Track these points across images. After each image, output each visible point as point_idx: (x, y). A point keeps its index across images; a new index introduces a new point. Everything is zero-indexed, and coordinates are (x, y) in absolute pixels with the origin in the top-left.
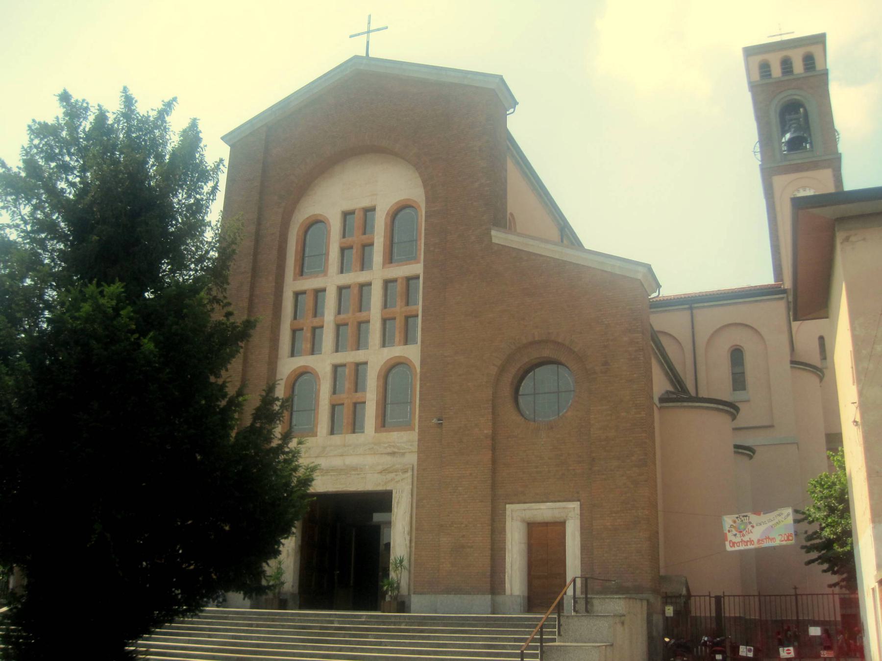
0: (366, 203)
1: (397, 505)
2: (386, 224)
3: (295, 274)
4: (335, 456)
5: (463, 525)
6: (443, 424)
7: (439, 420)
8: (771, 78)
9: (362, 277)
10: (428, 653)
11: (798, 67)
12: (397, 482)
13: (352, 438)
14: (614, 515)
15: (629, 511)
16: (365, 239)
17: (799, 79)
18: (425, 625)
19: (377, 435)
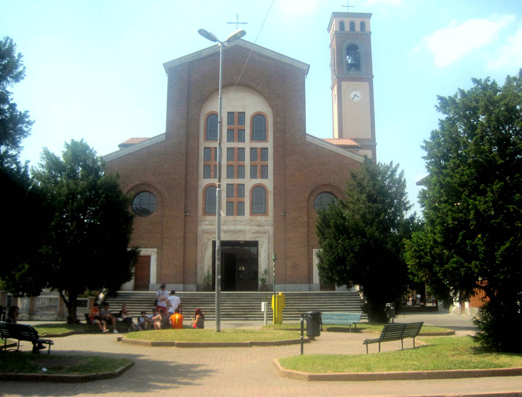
0: (241, 110)
3: (204, 139)
4: (231, 225)
7: (284, 213)
8: (344, 30)
9: (240, 145)
10: (121, 301)
12: (261, 237)
13: (239, 218)
17: (358, 34)
18: (306, 296)
19: (251, 217)
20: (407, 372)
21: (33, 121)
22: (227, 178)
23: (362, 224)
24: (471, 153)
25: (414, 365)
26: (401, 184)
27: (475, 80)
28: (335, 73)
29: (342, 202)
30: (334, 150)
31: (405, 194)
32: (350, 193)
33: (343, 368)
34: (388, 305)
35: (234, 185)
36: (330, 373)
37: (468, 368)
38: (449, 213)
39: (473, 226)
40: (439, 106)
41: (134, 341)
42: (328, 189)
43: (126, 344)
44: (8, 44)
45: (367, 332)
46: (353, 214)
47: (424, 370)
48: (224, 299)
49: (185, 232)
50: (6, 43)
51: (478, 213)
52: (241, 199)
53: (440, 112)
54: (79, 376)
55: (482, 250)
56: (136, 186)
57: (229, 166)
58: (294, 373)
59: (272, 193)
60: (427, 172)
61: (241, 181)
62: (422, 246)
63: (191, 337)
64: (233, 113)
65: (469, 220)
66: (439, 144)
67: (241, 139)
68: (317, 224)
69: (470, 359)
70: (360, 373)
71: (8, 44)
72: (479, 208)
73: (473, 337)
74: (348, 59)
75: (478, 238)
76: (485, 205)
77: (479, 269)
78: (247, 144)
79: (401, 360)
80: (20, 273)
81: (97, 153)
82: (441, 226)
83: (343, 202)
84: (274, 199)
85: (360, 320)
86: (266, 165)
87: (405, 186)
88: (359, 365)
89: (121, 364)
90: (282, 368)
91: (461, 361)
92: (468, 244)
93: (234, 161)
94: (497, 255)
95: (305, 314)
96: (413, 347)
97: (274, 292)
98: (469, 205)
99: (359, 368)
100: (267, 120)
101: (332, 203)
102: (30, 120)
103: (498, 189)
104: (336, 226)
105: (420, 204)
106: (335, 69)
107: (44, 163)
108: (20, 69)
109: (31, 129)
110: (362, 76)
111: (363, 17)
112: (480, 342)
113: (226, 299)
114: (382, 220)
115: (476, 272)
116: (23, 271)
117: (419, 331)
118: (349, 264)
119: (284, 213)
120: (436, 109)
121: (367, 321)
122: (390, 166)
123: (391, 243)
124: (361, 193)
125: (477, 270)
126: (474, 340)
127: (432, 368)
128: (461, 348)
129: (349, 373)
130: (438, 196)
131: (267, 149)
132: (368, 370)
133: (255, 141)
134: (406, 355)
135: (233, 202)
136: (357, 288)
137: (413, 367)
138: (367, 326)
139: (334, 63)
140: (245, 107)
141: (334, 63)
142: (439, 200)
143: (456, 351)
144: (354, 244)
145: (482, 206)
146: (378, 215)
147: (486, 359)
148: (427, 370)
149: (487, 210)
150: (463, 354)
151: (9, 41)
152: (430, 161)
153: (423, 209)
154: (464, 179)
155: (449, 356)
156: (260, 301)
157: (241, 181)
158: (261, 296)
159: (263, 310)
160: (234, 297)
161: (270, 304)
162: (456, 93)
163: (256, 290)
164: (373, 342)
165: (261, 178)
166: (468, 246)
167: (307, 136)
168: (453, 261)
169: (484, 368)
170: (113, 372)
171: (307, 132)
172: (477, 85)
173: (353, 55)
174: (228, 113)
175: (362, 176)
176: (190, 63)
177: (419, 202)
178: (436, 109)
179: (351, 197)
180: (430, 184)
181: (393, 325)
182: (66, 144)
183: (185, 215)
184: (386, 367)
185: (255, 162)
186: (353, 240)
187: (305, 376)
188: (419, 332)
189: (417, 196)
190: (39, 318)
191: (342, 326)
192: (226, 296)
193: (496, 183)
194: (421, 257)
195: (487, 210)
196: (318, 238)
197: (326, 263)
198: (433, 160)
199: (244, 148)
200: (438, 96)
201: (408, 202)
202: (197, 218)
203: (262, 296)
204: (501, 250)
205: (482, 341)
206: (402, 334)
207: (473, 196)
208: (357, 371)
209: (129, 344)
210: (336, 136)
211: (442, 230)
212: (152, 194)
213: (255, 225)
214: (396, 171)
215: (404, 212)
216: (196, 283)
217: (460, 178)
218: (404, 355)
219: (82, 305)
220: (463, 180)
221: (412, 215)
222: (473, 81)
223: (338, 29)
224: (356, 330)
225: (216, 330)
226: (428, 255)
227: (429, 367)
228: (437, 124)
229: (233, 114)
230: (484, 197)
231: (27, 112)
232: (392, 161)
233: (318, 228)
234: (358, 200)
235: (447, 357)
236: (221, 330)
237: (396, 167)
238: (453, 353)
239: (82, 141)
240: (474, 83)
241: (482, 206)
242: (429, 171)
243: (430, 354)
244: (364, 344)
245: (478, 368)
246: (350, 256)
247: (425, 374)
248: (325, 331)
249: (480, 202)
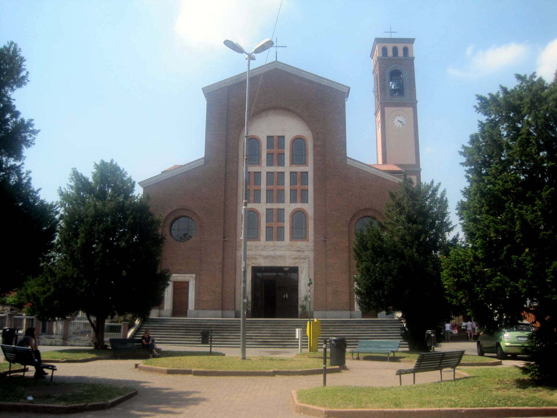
0: (280, 134)
2: (290, 145)
7: (324, 238)
8: (387, 56)
9: (280, 169)
11: (401, 54)
12: (301, 263)
16: (280, 151)
19: (291, 242)
20: (441, 409)
21: (37, 130)
22: (267, 202)
23: (400, 245)
24: (516, 156)
25: (451, 400)
26: (443, 203)
27: (519, 77)
28: (378, 99)
29: (380, 224)
30: (376, 174)
31: (447, 214)
32: (390, 214)
33: (367, 403)
34: (429, 332)
35: (274, 210)
36: (351, 408)
37: (515, 406)
38: (492, 224)
39: (519, 239)
40: (478, 106)
41: (150, 368)
42: (370, 214)
43: (142, 371)
44: (12, 49)
45: (406, 362)
46: (391, 235)
47: (462, 407)
48: (262, 326)
49: (223, 258)
50: (10, 48)
51: (524, 222)
52: (280, 224)
53: (480, 113)
54: (65, 406)
55: (530, 267)
56: (174, 211)
57: (269, 190)
58: (310, 408)
59: (313, 218)
60: (467, 182)
61: (281, 206)
62: (460, 263)
63: (211, 364)
64: (273, 137)
65: (514, 232)
66: (479, 149)
67: (281, 163)
68: (355, 247)
69: (518, 394)
70: (385, 410)
71: (13, 49)
72: (526, 218)
73: (521, 368)
74: (392, 84)
75: (525, 253)
76: (532, 214)
77: (526, 288)
78: (287, 169)
79: (436, 395)
80: (45, 296)
81: (127, 174)
82: (482, 240)
83: (381, 223)
84: (315, 223)
85: (399, 348)
86: (306, 189)
87: (447, 206)
88: (387, 399)
89: (119, 394)
90: (297, 402)
91: (507, 396)
92: (514, 259)
93: (273, 185)
94: (548, 272)
95: (328, 339)
96: (452, 379)
97: (309, 319)
98: (514, 214)
99: (386, 403)
100: (306, 143)
101: (369, 224)
102: (35, 129)
103: (548, 195)
104: (374, 248)
105: (458, 216)
106: (378, 95)
107: (72, 184)
108: (23, 74)
109: (35, 138)
110: (405, 102)
111: (407, 43)
112: (529, 374)
113: (264, 325)
114: (422, 241)
115: (523, 292)
116: (48, 294)
117: (459, 360)
118: (388, 288)
119: (324, 238)
120: (476, 110)
121: (407, 349)
122: (431, 185)
123: (432, 266)
124: (400, 213)
125: (524, 290)
126: (523, 372)
127: (472, 405)
128: (508, 381)
129: (373, 410)
130: (478, 206)
131: (307, 173)
132: (396, 405)
133: (295, 165)
134: (443, 389)
135: (273, 227)
136: (399, 315)
137: (449, 403)
138: (407, 355)
139: (378, 89)
141: (378, 89)
142: (479, 211)
143: (502, 383)
144: (393, 267)
145: (529, 216)
146: (418, 237)
147: (537, 395)
148: (466, 407)
149: (536, 221)
150: (509, 387)
151: (13, 46)
152: (469, 169)
153: (462, 221)
154: (508, 186)
155: (493, 390)
156: (293, 328)
157: (281, 206)
159: (297, 337)
160: (273, 324)
161: (304, 332)
162: (497, 92)
163: (297, 317)
164: (406, 372)
165: (301, 203)
166: (514, 262)
167: (348, 160)
168: (496, 280)
169: (536, 406)
170: (105, 403)
171: (348, 155)
172: (521, 82)
173: (396, 80)
174: (268, 137)
175: (401, 196)
176: (229, 87)
177: (457, 214)
178: (476, 110)
179: (390, 218)
180: (470, 195)
181: (433, 353)
182: (96, 165)
183: (224, 240)
184: (418, 402)
185: (295, 186)
186: (391, 263)
187: (321, 411)
188: (460, 362)
189: (455, 208)
190: (73, 343)
191: (380, 355)
192: (264, 323)
193: (545, 188)
194: (459, 276)
195: (536, 221)
196: (356, 262)
197: (363, 288)
198: (473, 167)
199: (284, 173)
200: (477, 95)
201: (450, 223)
202: (236, 243)
203: (301, 323)
204: (553, 266)
205: (532, 372)
206: (441, 364)
207: (519, 205)
208: (382, 407)
209: (145, 371)
210: (380, 162)
211: (483, 244)
212: (191, 218)
213: (295, 251)
214: (437, 191)
215: (447, 233)
216: (235, 309)
217: (503, 185)
218: (441, 388)
219: (117, 330)
220: (507, 187)
221: (455, 236)
222: (516, 77)
223: (381, 55)
224: (395, 359)
225: (241, 357)
226: (467, 274)
227: (468, 404)
228: (477, 126)
229: (272, 138)
230: (531, 206)
231: (32, 120)
232: (433, 180)
233: (355, 250)
234: (397, 221)
235: (491, 391)
236: (247, 358)
237: (437, 186)
238: (498, 386)
239: (112, 161)
240: (518, 80)
241: (529, 216)
242: (468, 181)
243: (471, 388)
244: (397, 374)
245: (528, 405)
246: (389, 280)
247: (463, 412)
248: (362, 360)
249: (527, 211)
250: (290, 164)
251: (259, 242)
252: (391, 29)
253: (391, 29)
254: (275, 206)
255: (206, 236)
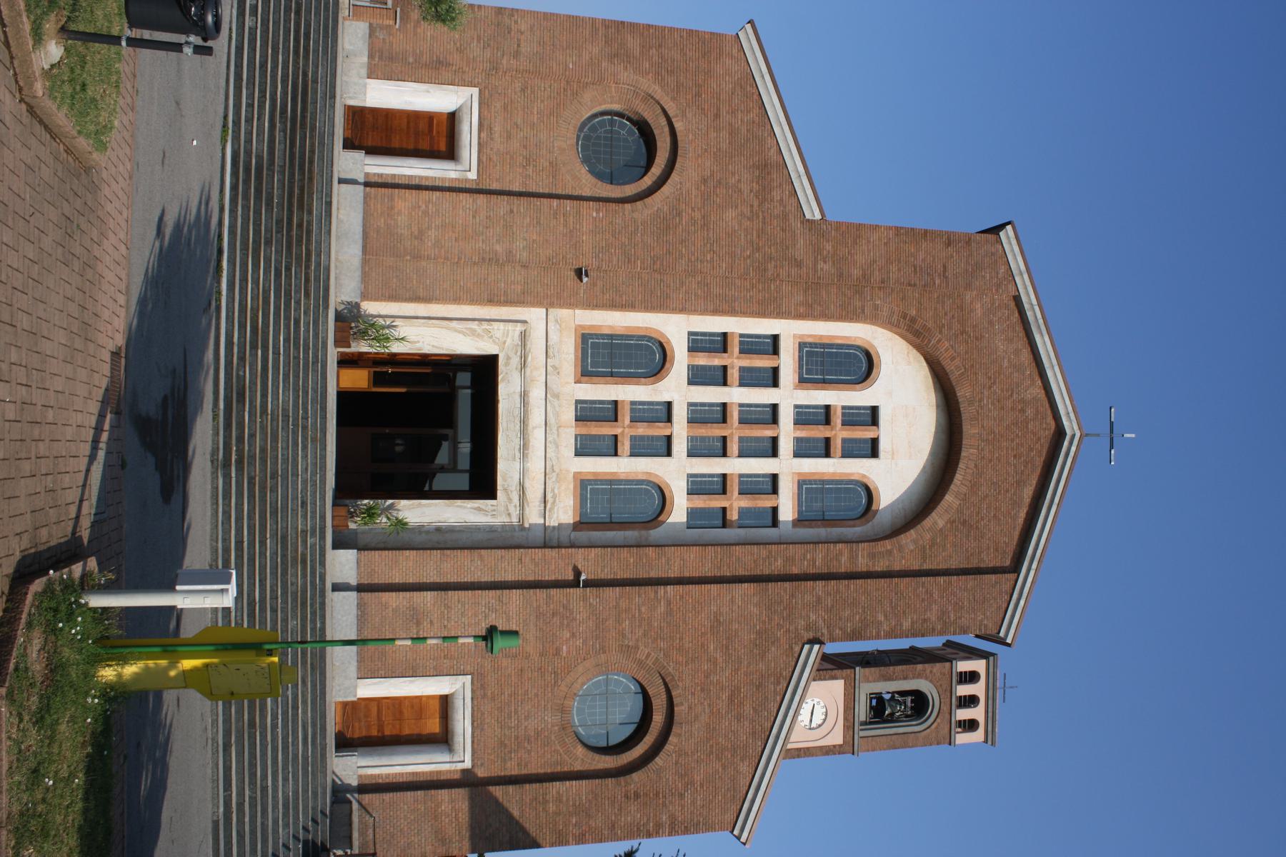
0: (883, 446)
1: (475, 509)
5: (446, 622)
6: (578, 589)
14: (454, 814)
15: (457, 832)
19: (571, 475)
140: (893, 458)
158: (314, 512)
250: (799, 474)
251: (572, 379)
252: (1011, 687)
253: (1011, 687)
254: (680, 430)
255: (594, 214)
